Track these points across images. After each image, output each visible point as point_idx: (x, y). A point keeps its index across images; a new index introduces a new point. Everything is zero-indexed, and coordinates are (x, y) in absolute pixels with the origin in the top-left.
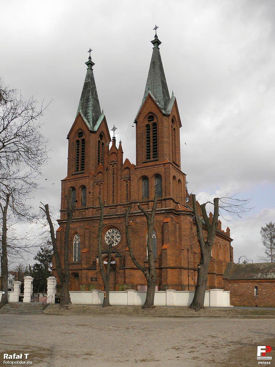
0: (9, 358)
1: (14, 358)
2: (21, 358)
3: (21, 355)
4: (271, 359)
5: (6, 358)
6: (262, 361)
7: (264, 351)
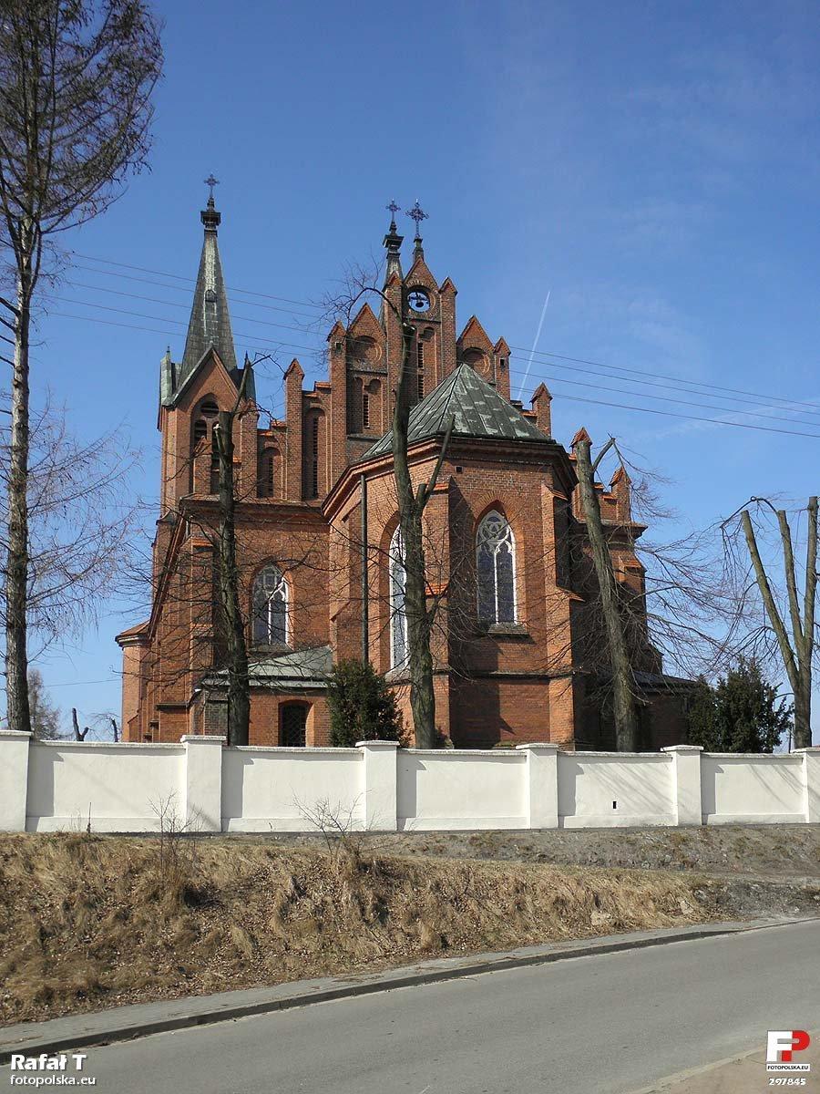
0: (27, 1067)
1: (42, 1067)
2: (63, 1068)
3: (63, 1057)
4: (808, 1070)
5: (17, 1066)
6: (777, 1076)
7: (788, 1047)
